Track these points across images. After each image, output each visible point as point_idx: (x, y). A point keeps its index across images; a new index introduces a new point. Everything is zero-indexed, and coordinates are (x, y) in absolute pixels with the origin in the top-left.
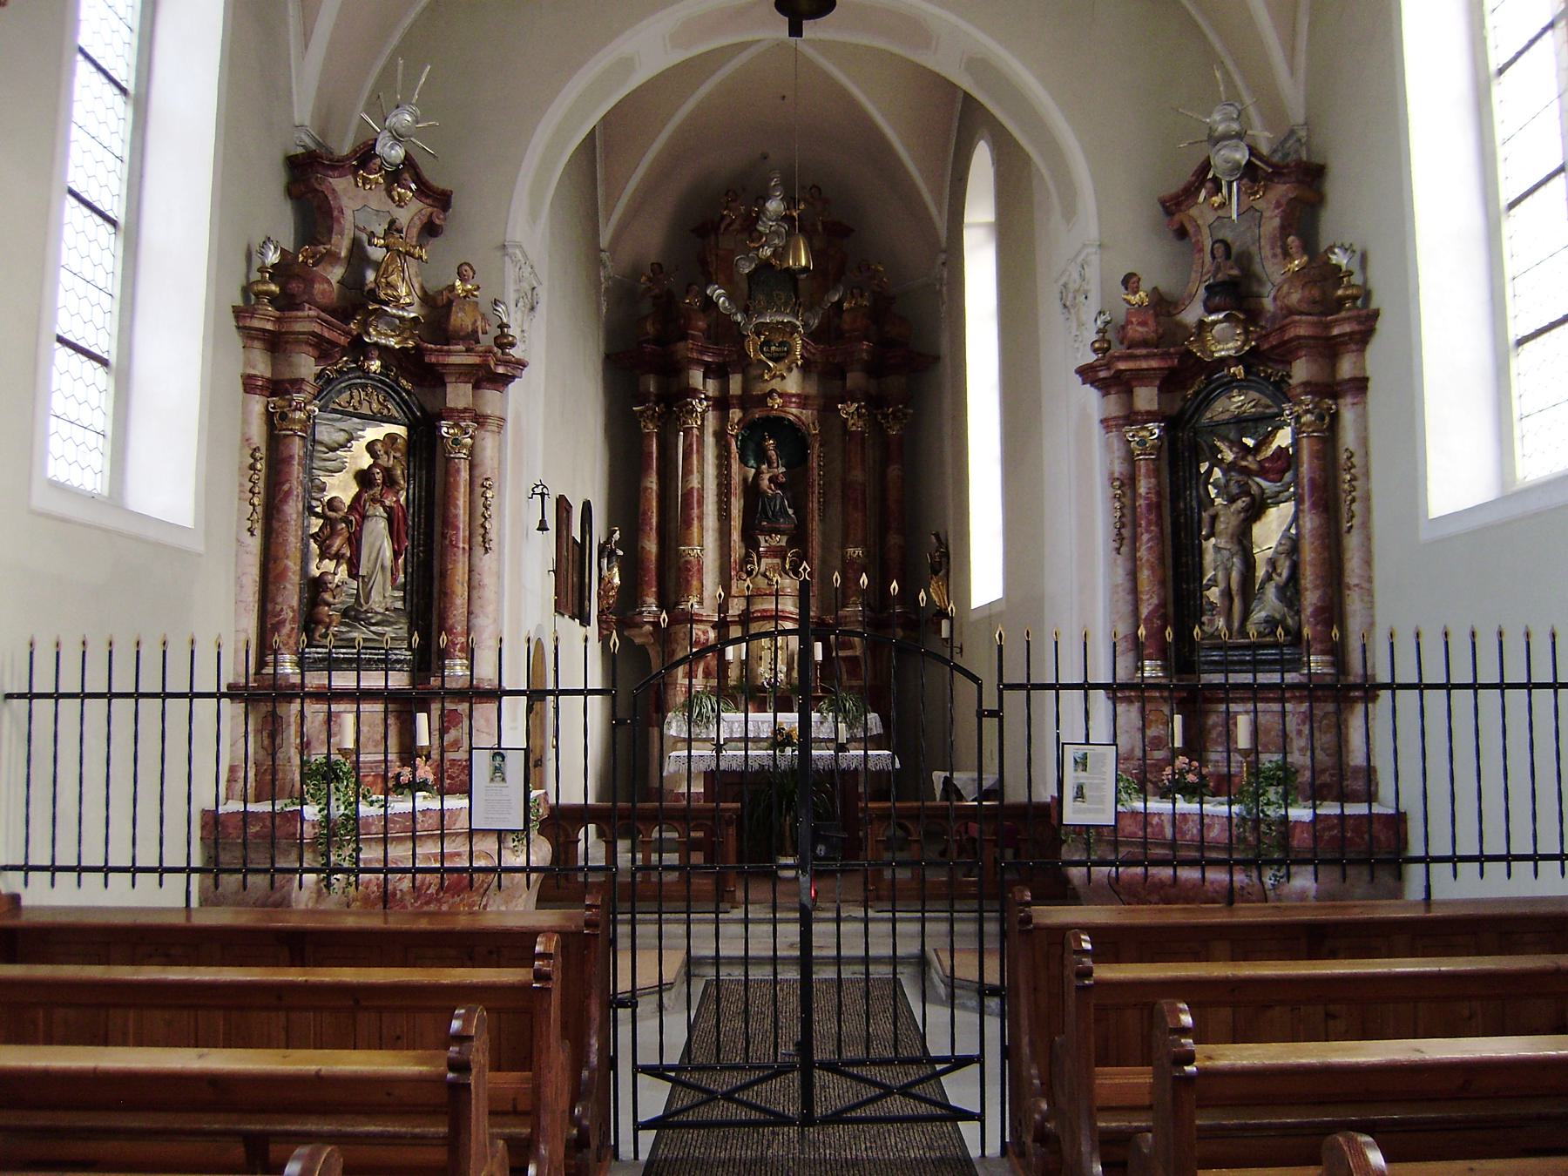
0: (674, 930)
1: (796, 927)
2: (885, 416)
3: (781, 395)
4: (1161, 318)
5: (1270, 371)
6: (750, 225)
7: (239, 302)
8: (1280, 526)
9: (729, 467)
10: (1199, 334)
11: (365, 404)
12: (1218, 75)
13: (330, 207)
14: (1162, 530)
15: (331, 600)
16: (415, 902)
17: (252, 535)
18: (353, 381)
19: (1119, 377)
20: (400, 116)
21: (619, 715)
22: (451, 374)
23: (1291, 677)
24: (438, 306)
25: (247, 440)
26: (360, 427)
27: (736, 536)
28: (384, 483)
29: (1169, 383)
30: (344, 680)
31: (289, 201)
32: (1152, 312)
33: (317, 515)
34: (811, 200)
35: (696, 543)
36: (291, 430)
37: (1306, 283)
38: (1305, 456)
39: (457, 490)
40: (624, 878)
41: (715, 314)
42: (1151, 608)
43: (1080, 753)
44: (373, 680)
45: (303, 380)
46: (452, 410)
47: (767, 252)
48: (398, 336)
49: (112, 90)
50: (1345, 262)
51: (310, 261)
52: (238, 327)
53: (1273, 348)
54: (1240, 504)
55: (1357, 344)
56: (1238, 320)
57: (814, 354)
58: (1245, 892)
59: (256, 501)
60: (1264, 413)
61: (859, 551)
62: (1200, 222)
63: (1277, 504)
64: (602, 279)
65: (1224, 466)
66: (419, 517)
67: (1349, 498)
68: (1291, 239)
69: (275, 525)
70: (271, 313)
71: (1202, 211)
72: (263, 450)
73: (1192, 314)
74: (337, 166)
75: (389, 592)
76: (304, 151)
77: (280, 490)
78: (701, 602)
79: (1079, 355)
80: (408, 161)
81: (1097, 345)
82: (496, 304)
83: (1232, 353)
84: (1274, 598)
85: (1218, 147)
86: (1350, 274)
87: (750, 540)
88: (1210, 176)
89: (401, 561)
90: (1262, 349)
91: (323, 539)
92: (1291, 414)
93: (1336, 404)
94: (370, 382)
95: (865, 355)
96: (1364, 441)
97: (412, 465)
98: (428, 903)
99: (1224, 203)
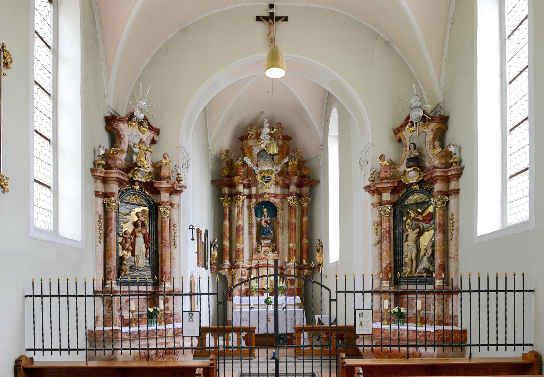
0: (237, 365)
1: (274, 364)
2: (302, 201)
3: (268, 194)
4: (392, 169)
5: (427, 187)
6: (258, 136)
7: (92, 167)
8: (429, 238)
9: (251, 218)
10: (404, 175)
11: (135, 200)
12: (414, 85)
13: (120, 134)
14: (390, 240)
15: (126, 263)
16: (156, 357)
17: (100, 243)
18: (130, 193)
19: (378, 190)
20: (142, 103)
21: (219, 301)
22: (162, 190)
23: (429, 287)
24: (157, 168)
25: (97, 212)
26: (133, 208)
27: (254, 240)
28: (142, 226)
29: (394, 191)
30: (134, 289)
31: (106, 132)
32: (389, 168)
33: (120, 236)
34: (278, 128)
35: (241, 242)
36: (111, 209)
37: (440, 158)
38: (437, 215)
39: (165, 227)
40: (221, 349)
41: (246, 167)
42: (386, 264)
43: (361, 312)
44: (143, 288)
45: (114, 193)
46: (163, 202)
47: (263, 146)
48: (144, 178)
49: (45, 94)
50: (453, 150)
51: (115, 153)
52: (92, 176)
53: (429, 179)
54: (416, 231)
55: (456, 178)
56: (417, 170)
57: (279, 180)
58: (414, 354)
59: (101, 232)
60: (425, 201)
61: (294, 245)
62: (406, 137)
63: (428, 231)
64: (210, 156)
65: (411, 218)
66: (154, 237)
67: (452, 229)
68: (436, 142)
69: (108, 240)
70: (103, 171)
71: (407, 133)
72: (103, 215)
73: (402, 168)
74: (121, 120)
75: (145, 261)
76: (111, 115)
77: (108, 229)
78: (243, 262)
79: (365, 182)
80: (145, 118)
81: (371, 179)
82: (176, 167)
83: (415, 181)
84: (426, 261)
85: (413, 111)
86: (455, 154)
87: (258, 240)
88: (410, 121)
89: (148, 251)
90: (425, 180)
91: (123, 244)
92: (434, 201)
93: (449, 198)
94: (136, 193)
95: (296, 181)
96: (458, 211)
97: (150, 220)
98: (160, 358)
99: (414, 130)
